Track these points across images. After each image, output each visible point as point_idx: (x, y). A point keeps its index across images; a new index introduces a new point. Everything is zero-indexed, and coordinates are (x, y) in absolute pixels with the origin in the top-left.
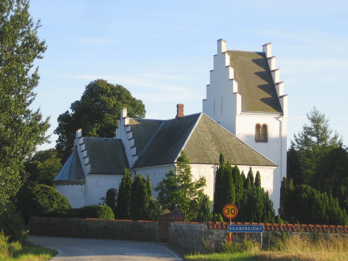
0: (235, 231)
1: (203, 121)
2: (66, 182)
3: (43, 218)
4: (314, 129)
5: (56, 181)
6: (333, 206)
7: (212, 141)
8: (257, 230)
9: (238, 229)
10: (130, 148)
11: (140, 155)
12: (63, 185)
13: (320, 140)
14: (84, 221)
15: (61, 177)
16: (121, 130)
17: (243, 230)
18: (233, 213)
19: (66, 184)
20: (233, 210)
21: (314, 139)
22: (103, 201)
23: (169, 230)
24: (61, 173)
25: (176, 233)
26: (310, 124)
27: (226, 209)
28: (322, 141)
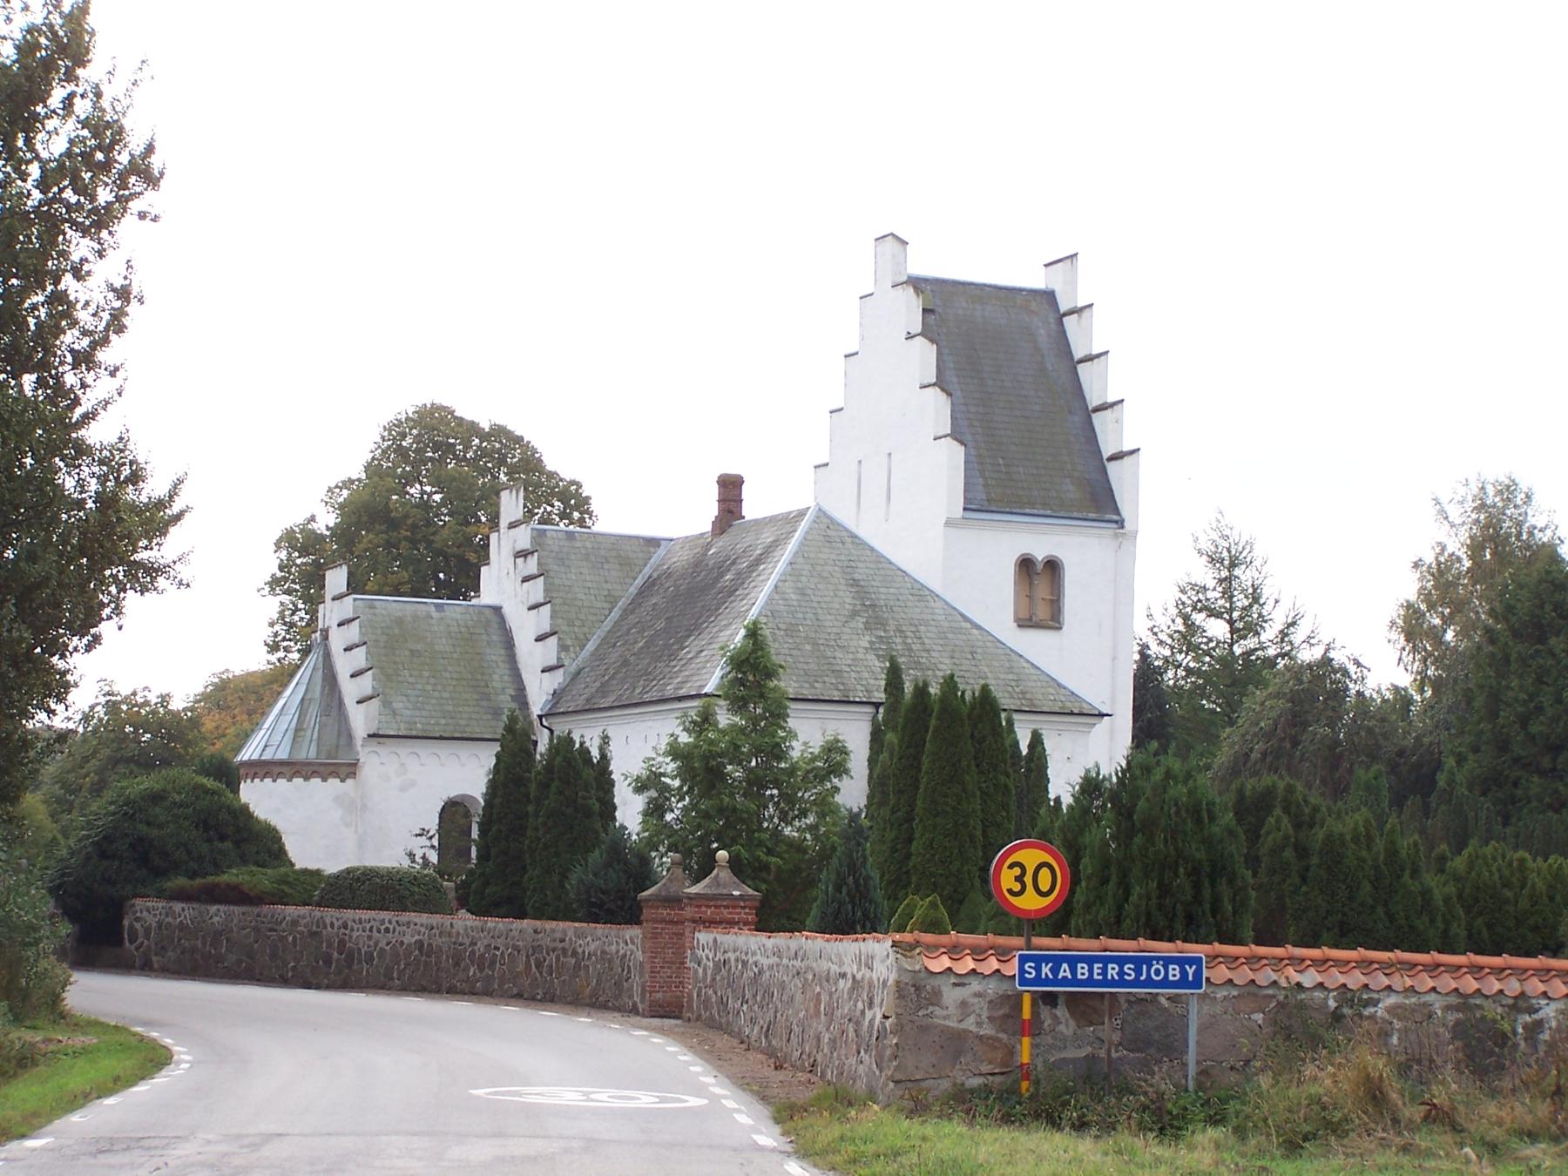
0: (1056, 982)
1: (822, 538)
2: (284, 769)
3: (178, 906)
4: (1214, 589)
5: (250, 764)
6: (1403, 870)
7: (854, 614)
8: (1171, 978)
9: (1069, 975)
10: (540, 669)
11: (573, 668)
12: (272, 777)
13: (1237, 633)
14: (338, 920)
15: (266, 746)
16: (499, 570)
17: (1096, 977)
18: (1044, 887)
19: (280, 775)
20: (1045, 874)
21: (1217, 629)
22: (423, 841)
23: (690, 964)
24: (263, 732)
25: (718, 978)
26: (1206, 576)
27: (1011, 867)
28: (1244, 637)
